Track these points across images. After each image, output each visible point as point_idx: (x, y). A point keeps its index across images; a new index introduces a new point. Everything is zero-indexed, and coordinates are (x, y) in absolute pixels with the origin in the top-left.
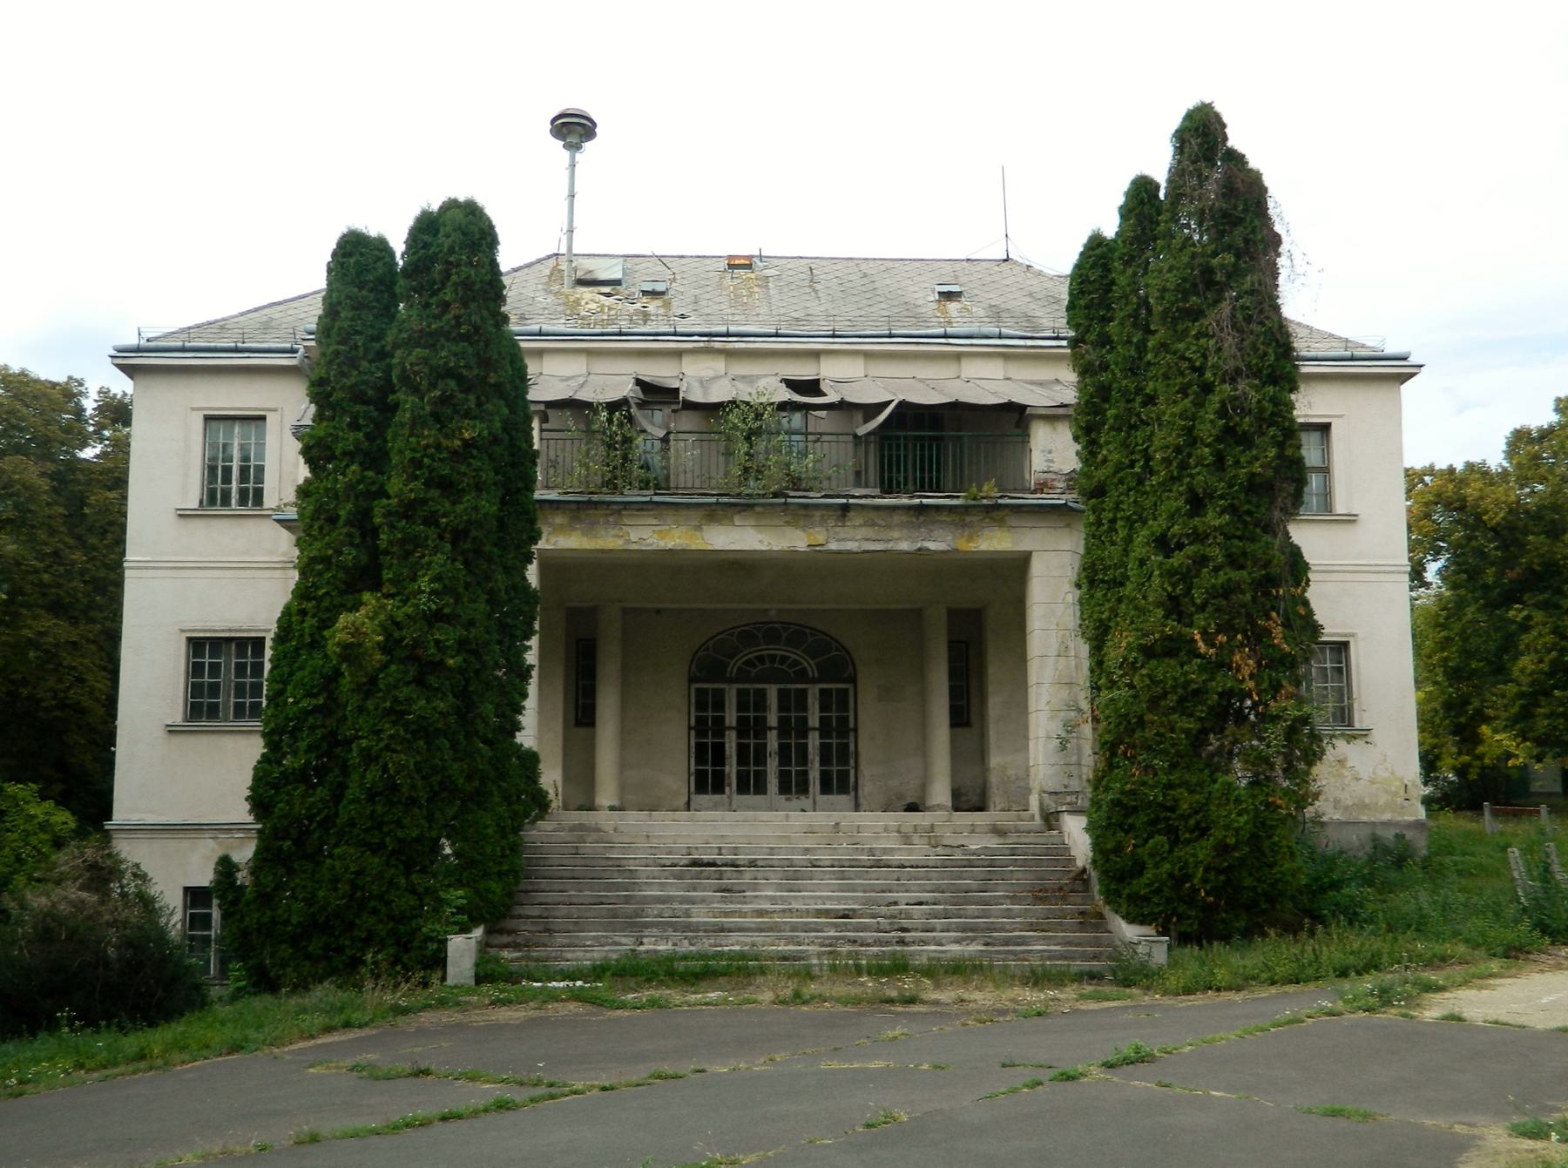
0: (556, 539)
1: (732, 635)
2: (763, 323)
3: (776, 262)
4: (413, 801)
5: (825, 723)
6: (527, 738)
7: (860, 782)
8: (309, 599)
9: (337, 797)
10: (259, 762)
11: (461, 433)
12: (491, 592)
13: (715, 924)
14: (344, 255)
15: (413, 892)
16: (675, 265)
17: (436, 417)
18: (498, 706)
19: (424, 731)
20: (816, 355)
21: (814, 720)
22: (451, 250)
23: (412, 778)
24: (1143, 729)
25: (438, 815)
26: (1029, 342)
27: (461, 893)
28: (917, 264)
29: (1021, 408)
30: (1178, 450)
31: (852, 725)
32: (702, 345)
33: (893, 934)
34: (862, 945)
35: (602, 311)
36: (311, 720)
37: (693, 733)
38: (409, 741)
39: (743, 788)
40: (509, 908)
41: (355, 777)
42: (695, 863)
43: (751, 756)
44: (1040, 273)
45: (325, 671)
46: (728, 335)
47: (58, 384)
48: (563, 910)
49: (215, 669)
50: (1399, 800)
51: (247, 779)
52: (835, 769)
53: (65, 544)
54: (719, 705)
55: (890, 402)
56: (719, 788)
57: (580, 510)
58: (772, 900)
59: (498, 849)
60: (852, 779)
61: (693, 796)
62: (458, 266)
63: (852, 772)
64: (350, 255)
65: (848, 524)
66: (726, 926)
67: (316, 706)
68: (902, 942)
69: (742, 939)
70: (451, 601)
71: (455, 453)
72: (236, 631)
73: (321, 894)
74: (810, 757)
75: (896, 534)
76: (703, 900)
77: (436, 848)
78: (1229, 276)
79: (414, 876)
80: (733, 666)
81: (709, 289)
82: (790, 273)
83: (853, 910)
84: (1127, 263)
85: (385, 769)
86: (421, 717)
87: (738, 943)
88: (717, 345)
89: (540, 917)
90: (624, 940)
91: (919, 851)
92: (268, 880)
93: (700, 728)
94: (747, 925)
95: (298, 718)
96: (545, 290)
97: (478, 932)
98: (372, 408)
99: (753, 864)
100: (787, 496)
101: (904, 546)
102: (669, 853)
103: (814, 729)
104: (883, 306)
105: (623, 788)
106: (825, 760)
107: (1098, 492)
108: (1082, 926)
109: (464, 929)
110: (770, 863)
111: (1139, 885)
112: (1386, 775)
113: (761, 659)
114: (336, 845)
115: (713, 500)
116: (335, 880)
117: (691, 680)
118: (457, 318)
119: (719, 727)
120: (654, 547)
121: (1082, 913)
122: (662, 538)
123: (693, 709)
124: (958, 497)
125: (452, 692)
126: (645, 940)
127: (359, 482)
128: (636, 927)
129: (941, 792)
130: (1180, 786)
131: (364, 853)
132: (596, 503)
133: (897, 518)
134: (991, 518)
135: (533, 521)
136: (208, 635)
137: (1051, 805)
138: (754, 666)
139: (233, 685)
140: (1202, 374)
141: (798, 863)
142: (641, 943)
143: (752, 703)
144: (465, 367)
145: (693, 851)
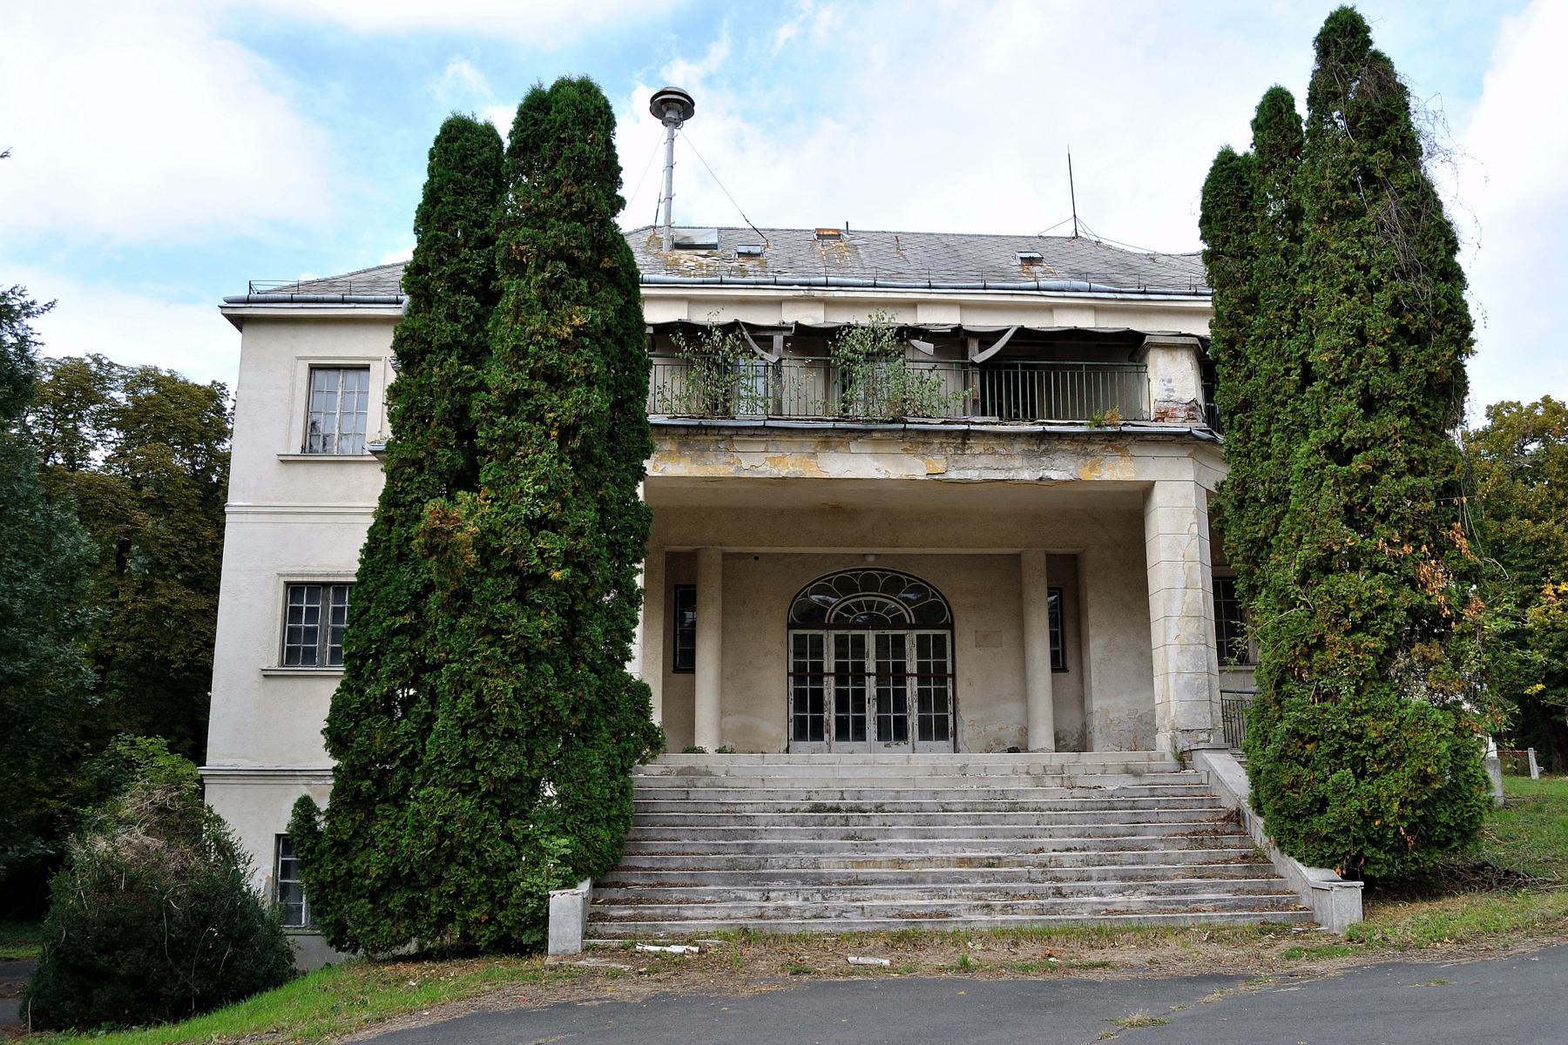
0: (663, 466)
3: (862, 235)
4: (510, 735)
6: (633, 669)
7: (959, 729)
8: (397, 506)
9: (425, 732)
11: (571, 319)
12: (601, 501)
13: (849, 876)
14: (448, 141)
15: (508, 838)
17: (545, 303)
18: (607, 632)
19: (529, 655)
20: (913, 305)
21: (912, 666)
22: (564, 126)
23: (510, 707)
24: (1323, 651)
25: (539, 752)
26: (1119, 296)
27: (564, 841)
28: (994, 239)
30: (1347, 350)
31: (949, 671)
32: (802, 293)
36: (397, 641)
37: (791, 678)
38: (507, 665)
39: (842, 734)
40: (617, 858)
41: (444, 705)
42: (817, 808)
43: (850, 701)
44: (1109, 248)
45: (413, 586)
46: (827, 285)
47: (203, 387)
48: (678, 861)
49: (312, 613)
53: (200, 522)
54: (818, 652)
55: (1004, 332)
56: (818, 735)
57: (689, 435)
58: (907, 847)
59: (607, 791)
60: (951, 725)
62: (571, 141)
63: (951, 718)
64: (455, 139)
66: (861, 878)
67: (403, 625)
69: (881, 892)
70: (558, 505)
71: (565, 342)
72: (334, 575)
73: (404, 842)
74: (909, 702)
75: (1017, 463)
76: (831, 849)
77: (534, 789)
78: (1387, 172)
79: (510, 822)
81: (802, 253)
82: (877, 243)
85: (479, 694)
86: (520, 636)
87: (877, 897)
88: (817, 294)
89: (651, 869)
90: (749, 895)
91: (1054, 793)
92: (346, 828)
93: (798, 674)
94: (884, 877)
95: (382, 641)
97: (584, 887)
99: (879, 808)
100: (906, 422)
101: (1026, 475)
102: (788, 798)
105: (722, 733)
108: (1250, 873)
109: (568, 883)
111: (1320, 824)
113: (859, 605)
114: (422, 786)
115: (830, 425)
116: (420, 827)
117: (791, 626)
118: (568, 196)
119: (818, 673)
120: (767, 475)
121: (1244, 857)
122: (775, 466)
123: (791, 656)
124: (1081, 424)
125: (557, 611)
126: (772, 895)
127: (456, 377)
128: (758, 877)
129: (1043, 735)
130: (1366, 712)
131: (453, 794)
132: (706, 427)
133: (1018, 447)
134: (1113, 447)
136: (306, 579)
137: (1184, 743)
138: (852, 613)
139: (329, 630)
140: (1367, 272)
141: (928, 807)
142: (768, 899)
143: (850, 648)
144: (577, 247)
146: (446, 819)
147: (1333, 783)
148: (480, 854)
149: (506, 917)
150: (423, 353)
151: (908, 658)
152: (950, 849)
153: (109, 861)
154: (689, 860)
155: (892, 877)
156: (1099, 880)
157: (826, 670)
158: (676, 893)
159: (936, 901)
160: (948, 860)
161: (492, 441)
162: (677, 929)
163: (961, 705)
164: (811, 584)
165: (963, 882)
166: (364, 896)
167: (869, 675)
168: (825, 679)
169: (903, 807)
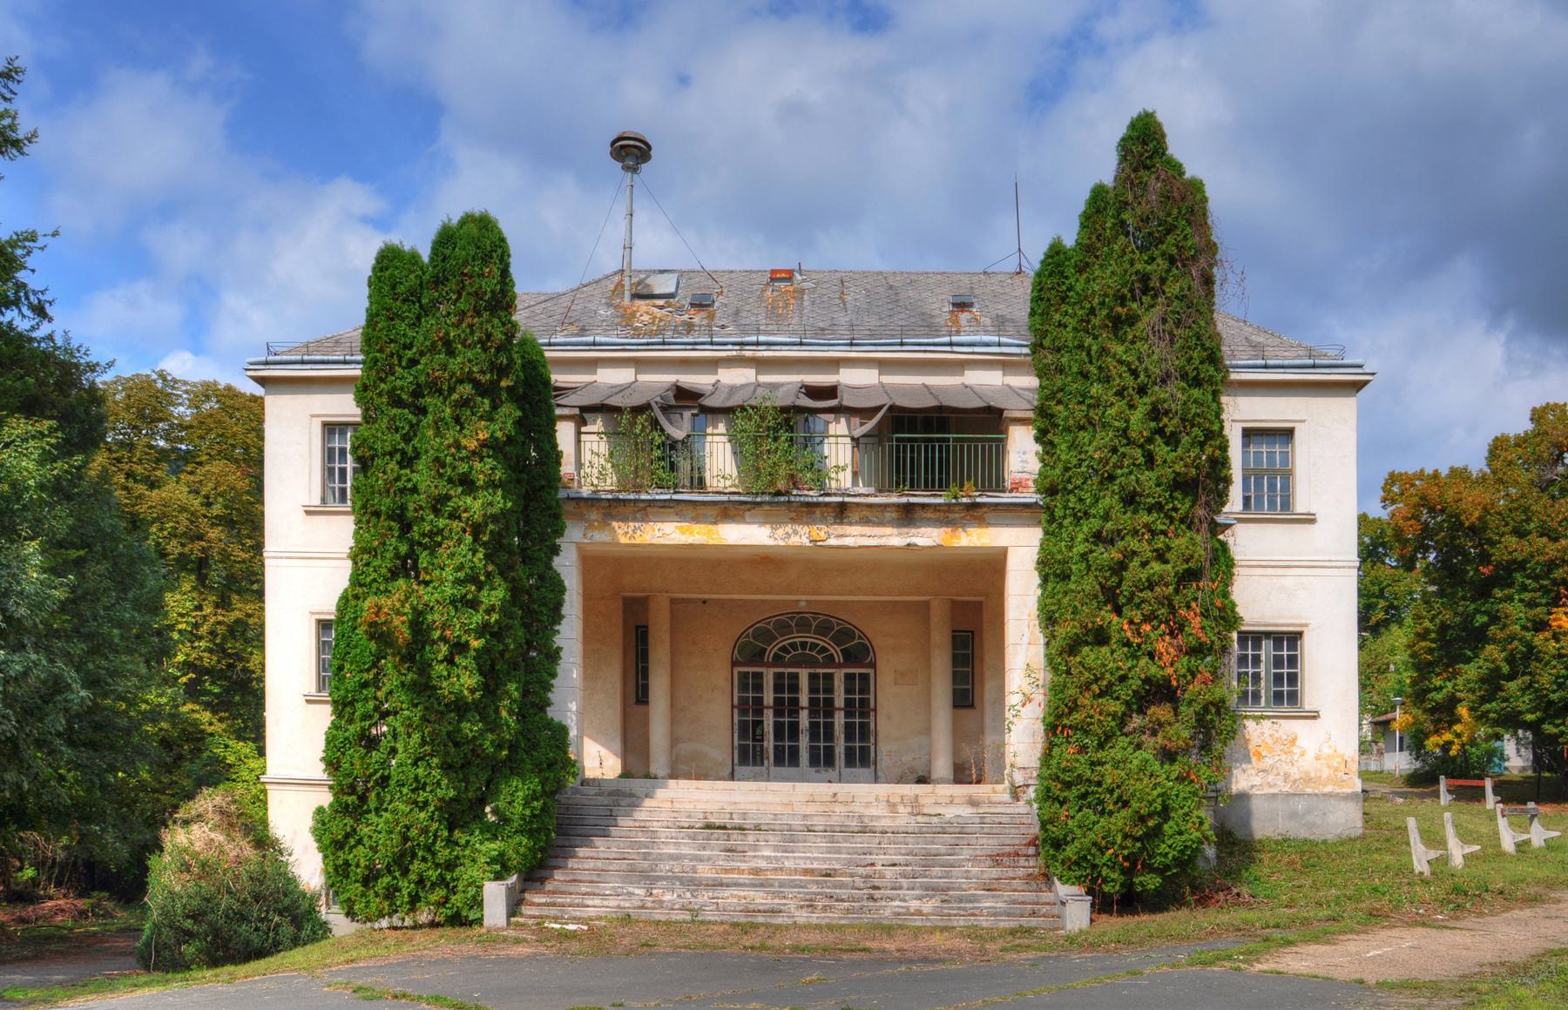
1: (768, 623)
2: (793, 333)
5: (849, 703)
7: (878, 758)
10: (330, 728)
14: (381, 270)
16: (723, 281)
17: (457, 420)
20: (835, 364)
21: (839, 701)
22: (466, 263)
29: (1000, 411)
31: (872, 705)
32: (734, 353)
33: (865, 891)
34: (837, 900)
35: (653, 323)
37: (736, 711)
39: (779, 761)
42: (708, 826)
50: (1340, 774)
51: (321, 744)
52: (822, 745)
54: (759, 687)
60: (872, 755)
61: (736, 768)
63: (872, 748)
65: (846, 520)
66: (724, 881)
68: (871, 898)
69: (735, 893)
74: (837, 734)
75: (888, 530)
76: (709, 859)
80: (769, 656)
83: (835, 870)
84: (1080, 271)
88: (748, 354)
90: (637, 891)
91: (903, 819)
93: (743, 706)
96: (607, 304)
98: (407, 411)
99: (757, 828)
102: (689, 817)
103: (840, 709)
104: (901, 316)
106: (849, 736)
107: (1051, 491)
110: (772, 827)
112: (1330, 752)
113: (793, 646)
117: (734, 664)
123: (736, 690)
124: (941, 496)
129: (942, 765)
135: (557, 517)
141: (797, 828)
145: (709, 816)
146: (408, 828)
147: (1079, 821)
148: (434, 854)
149: (456, 900)
150: (372, 458)
151: (836, 694)
152: (802, 862)
153: (186, 850)
154: (599, 864)
155: (747, 881)
156: (908, 889)
157: (765, 703)
158: (584, 888)
159: (777, 901)
160: (796, 870)
161: (424, 535)
162: (578, 914)
163: (880, 736)
164: (751, 627)
165: (802, 887)
166: (358, 881)
167: (802, 708)
168: (765, 711)
169: (777, 827)
